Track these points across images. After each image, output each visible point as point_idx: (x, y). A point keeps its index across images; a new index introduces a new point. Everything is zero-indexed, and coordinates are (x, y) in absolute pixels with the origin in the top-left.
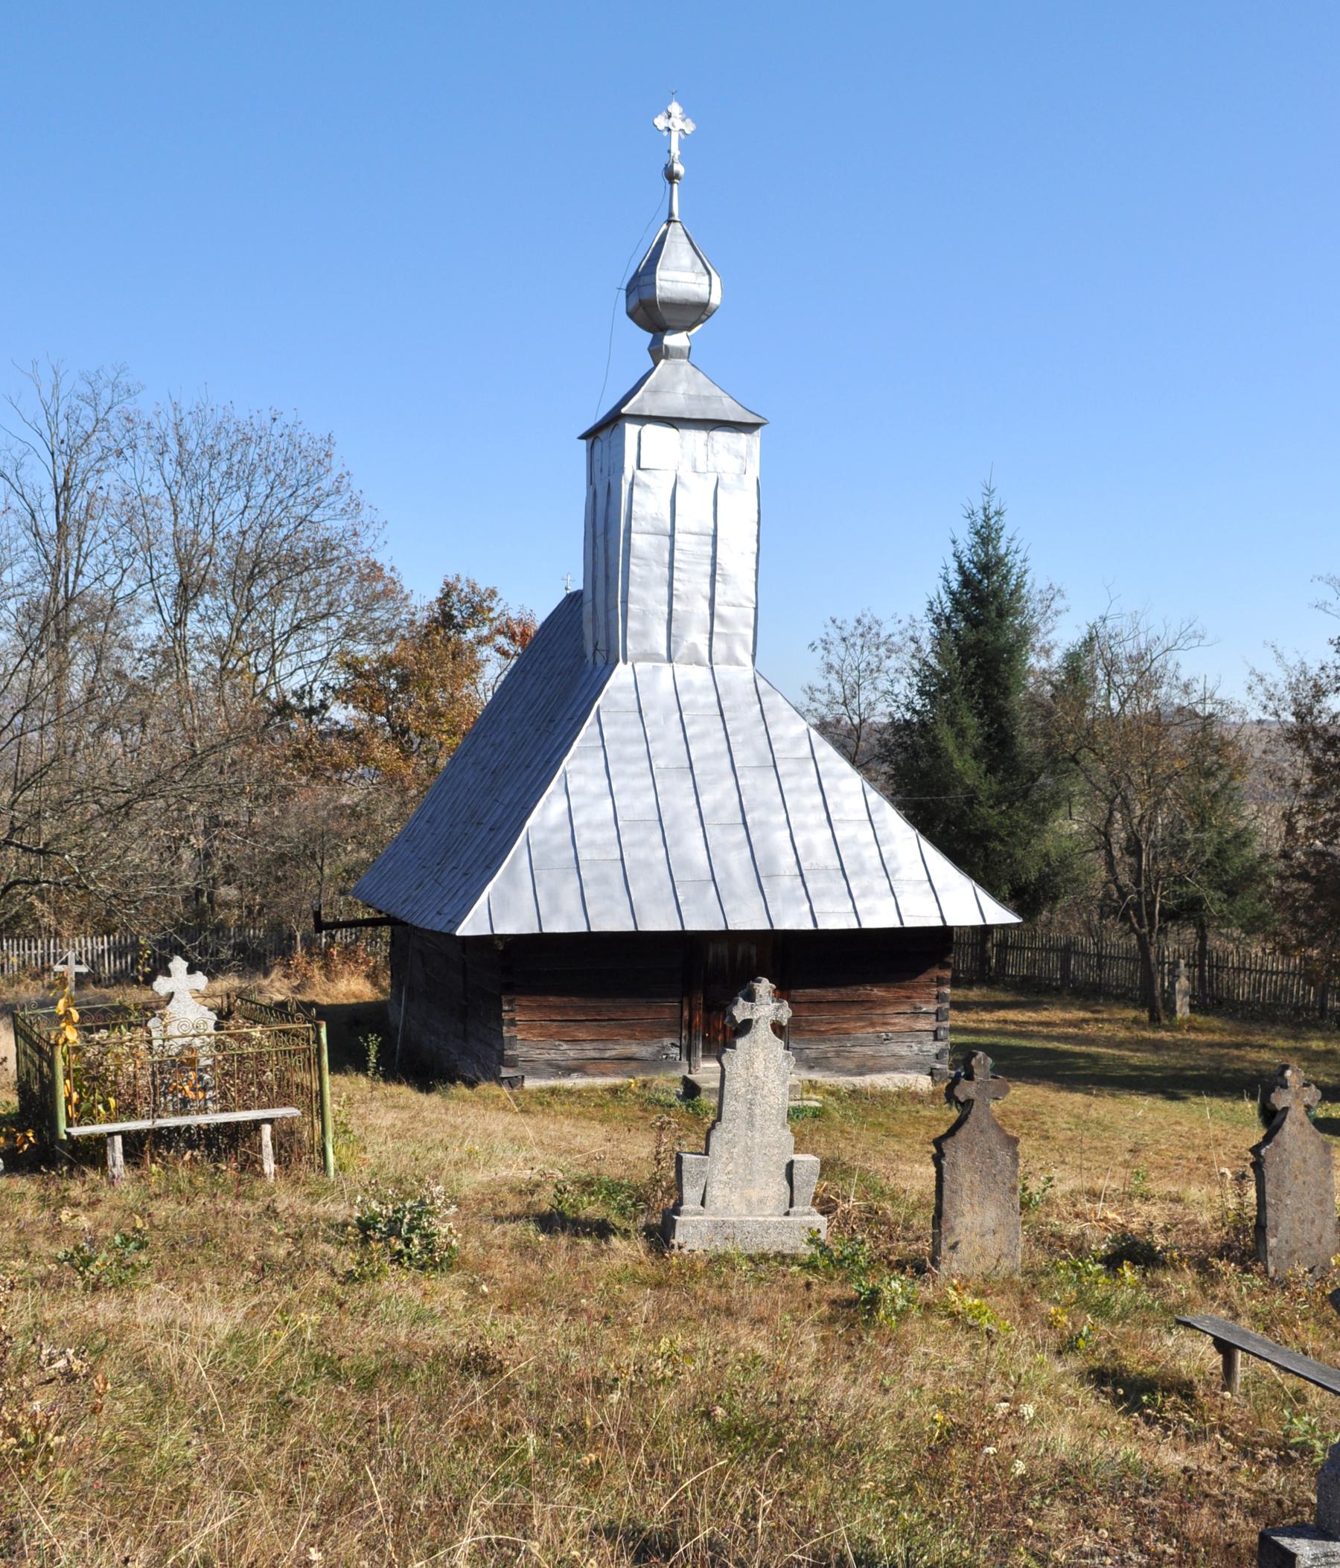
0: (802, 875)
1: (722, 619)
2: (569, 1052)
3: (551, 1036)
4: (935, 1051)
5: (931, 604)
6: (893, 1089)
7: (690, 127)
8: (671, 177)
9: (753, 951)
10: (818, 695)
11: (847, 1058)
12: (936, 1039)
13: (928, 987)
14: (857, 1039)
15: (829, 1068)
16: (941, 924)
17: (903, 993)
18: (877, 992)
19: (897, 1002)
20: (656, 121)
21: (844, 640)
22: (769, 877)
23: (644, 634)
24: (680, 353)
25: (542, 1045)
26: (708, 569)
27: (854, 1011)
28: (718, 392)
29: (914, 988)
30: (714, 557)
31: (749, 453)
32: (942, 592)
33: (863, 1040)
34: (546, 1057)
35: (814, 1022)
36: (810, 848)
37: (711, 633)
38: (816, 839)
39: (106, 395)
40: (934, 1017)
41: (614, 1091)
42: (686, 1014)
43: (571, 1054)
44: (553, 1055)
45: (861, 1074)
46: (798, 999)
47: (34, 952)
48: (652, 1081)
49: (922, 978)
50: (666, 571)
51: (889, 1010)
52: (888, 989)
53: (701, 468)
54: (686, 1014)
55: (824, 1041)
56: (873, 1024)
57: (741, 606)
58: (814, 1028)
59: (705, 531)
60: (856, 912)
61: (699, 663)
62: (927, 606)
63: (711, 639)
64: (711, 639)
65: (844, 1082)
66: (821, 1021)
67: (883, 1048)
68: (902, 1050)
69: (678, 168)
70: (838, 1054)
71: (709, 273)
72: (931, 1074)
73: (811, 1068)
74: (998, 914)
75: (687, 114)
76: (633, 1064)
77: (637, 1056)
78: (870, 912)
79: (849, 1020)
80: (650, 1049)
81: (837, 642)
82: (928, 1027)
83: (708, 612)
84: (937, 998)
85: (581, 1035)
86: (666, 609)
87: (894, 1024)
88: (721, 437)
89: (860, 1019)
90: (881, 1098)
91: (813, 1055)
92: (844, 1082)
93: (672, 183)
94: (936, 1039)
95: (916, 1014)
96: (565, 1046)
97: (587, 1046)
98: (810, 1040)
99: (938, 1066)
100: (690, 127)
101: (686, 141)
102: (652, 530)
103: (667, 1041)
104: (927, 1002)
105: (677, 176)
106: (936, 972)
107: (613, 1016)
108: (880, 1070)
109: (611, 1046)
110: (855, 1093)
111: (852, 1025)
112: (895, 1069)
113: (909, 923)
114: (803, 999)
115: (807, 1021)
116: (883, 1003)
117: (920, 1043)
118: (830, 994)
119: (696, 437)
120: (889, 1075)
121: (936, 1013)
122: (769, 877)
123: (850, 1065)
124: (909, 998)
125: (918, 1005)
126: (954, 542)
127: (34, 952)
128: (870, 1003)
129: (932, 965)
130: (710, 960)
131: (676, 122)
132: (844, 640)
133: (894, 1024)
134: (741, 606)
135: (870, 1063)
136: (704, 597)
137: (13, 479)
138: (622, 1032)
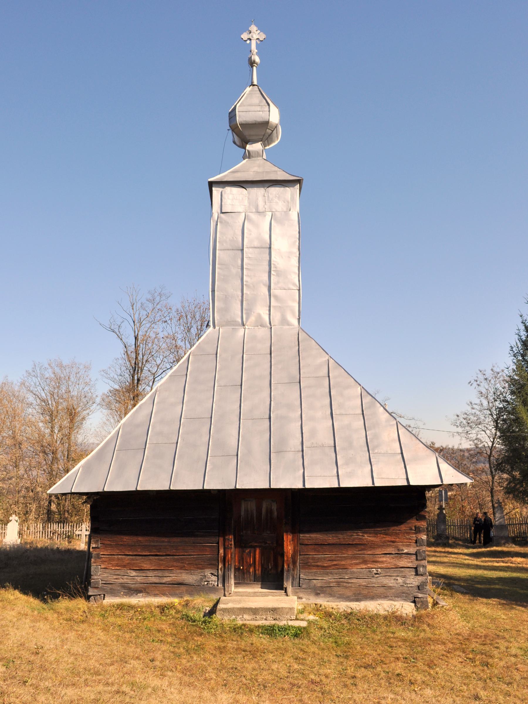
0: (303, 451)
1: (276, 297)
2: (133, 577)
3: (124, 566)
4: (417, 584)
5: (512, 347)
6: (382, 612)
7: (262, 37)
8: (252, 63)
9: (274, 507)
10: (475, 406)
11: (346, 587)
12: (417, 574)
13: (408, 533)
14: (353, 573)
15: (331, 595)
16: (406, 484)
17: (388, 538)
18: (368, 537)
19: (384, 545)
20: (242, 36)
21: (486, 379)
22: (278, 452)
23: (226, 310)
24: (258, 154)
25: (118, 573)
26: (267, 268)
27: (350, 552)
28: (276, 169)
29: (397, 534)
30: (270, 261)
31: (293, 198)
32: (518, 342)
33: (358, 574)
34: (121, 581)
35: (319, 560)
36: (313, 432)
37: (270, 307)
38: (320, 429)
39: (158, 299)
40: (414, 557)
41: (162, 608)
42: (221, 551)
43: (139, 579)
44: (125, 580)
45: (358, 600)
46: (306, 542)
47: (65, 529)
48: (192, 601)
49: (403, 527)
50: (240, 270)
51: (378, 551)
52: (376, 534)
53: (261, 209)
54: (221, 551)
55: (327, 574)
56: (365, 562)
57: (289, 289)
58: (319, 564)
59: (264, 246)
60: (338, 476)
61: (262, 326)
62: (510, 348)
63: (270, 310)
64: (270, 310)
65: (343, 606)
66: (325, 559)
67: (374, 580)
68: (390, 582)
69: (257, 59)
70: (339, 584)
71: (269, 105)
72: (414, 602)
73: (317, 594)
74: (461, 479)
75: (261, 28)
76: (183, 588)
77: (186, 582)
78: (350, 475)
79: (346, 558)
80: (195, 577)
81: (483, 380)
82: (410, 565)
83: (267, 293)
84: (416, 542)
85: (146, 566)
86: (240, 294)
87: (382, 562)
88: (274, 191)
89: (354, 557)
90: (370, 620)
91: (319, 585)
92: (343, 606)
93: (252, 67)
94: (417, 574)
95: (400, 554)
96: (134, 573)
97: (150, 574)
98: (316, 573)
99: (420, 595)
100: (262, 37)
101: (261, 43)
102: (231, 248)
103: (208, 572)
104: (408, 546)
105: (254, 62)
106: (414, 523)
107: (168, 553)
108: (372, 598)
109: (167, 574)
110: (348, 616)
111: (349, 562)
112: (385, 597)
113: (378, 484)
114: (310, 542)
115: (313, 559)
116: (373, 546)
117: (404, 577)
118: (330, 538)
119: (258, 192)
120: (380, 602)
121: (416, 554)
122: (278, 452)
123: (348, 593)
124: (393, 542)
125: (401, 548)
126: (521, 316)
127: (62, 530)
128: (363, 546)
129: (410, 517)
130: (243, 513)
131: (256, 34)
132: (486, 379)
133: (382, 562)
134: (289, 289)
135: (365, 592)
136: (264, 285)
137: (118, 333)
138: (175, 564)
